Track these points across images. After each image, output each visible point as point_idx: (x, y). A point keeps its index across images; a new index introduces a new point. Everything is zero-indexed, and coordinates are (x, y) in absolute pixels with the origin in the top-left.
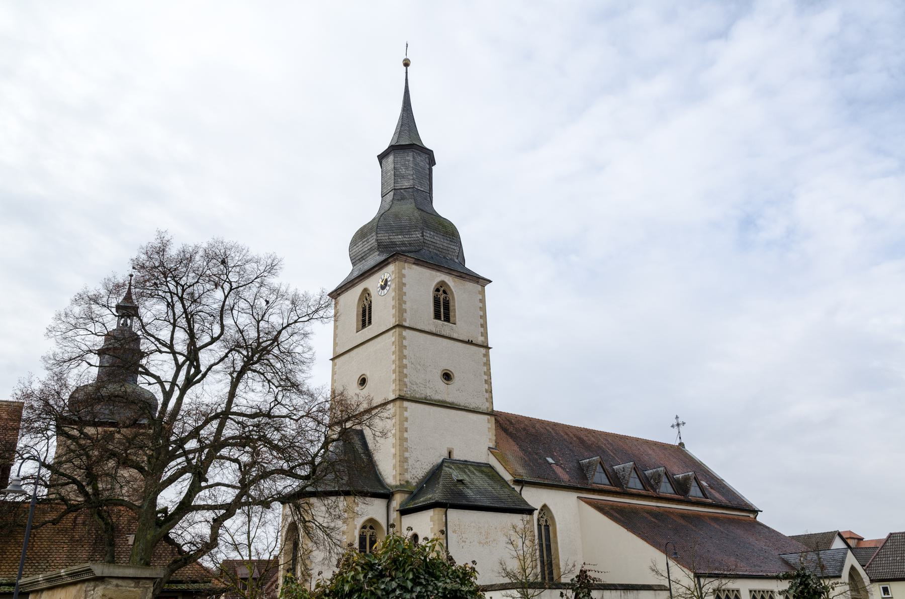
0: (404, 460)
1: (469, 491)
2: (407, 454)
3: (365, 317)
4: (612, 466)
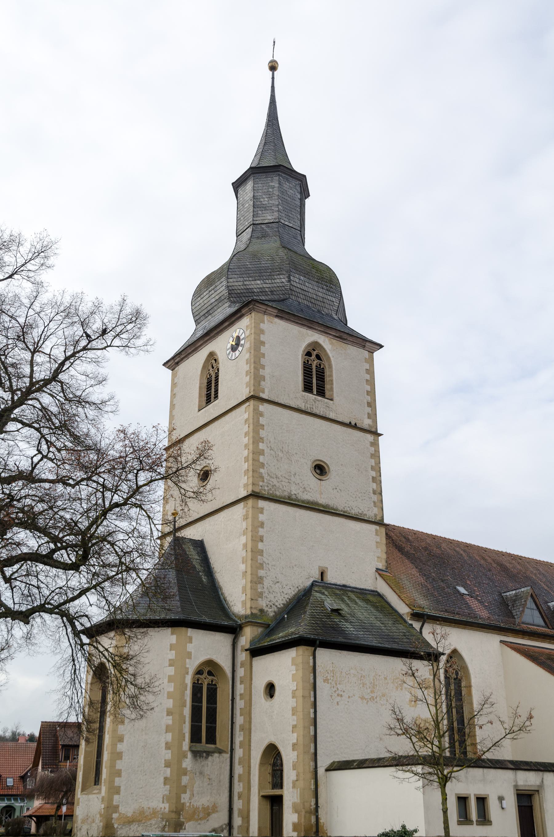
0: (257, 580)
1: (348, 625)
2: (261, 573)
3: (210, 390)
4: (547, 602)
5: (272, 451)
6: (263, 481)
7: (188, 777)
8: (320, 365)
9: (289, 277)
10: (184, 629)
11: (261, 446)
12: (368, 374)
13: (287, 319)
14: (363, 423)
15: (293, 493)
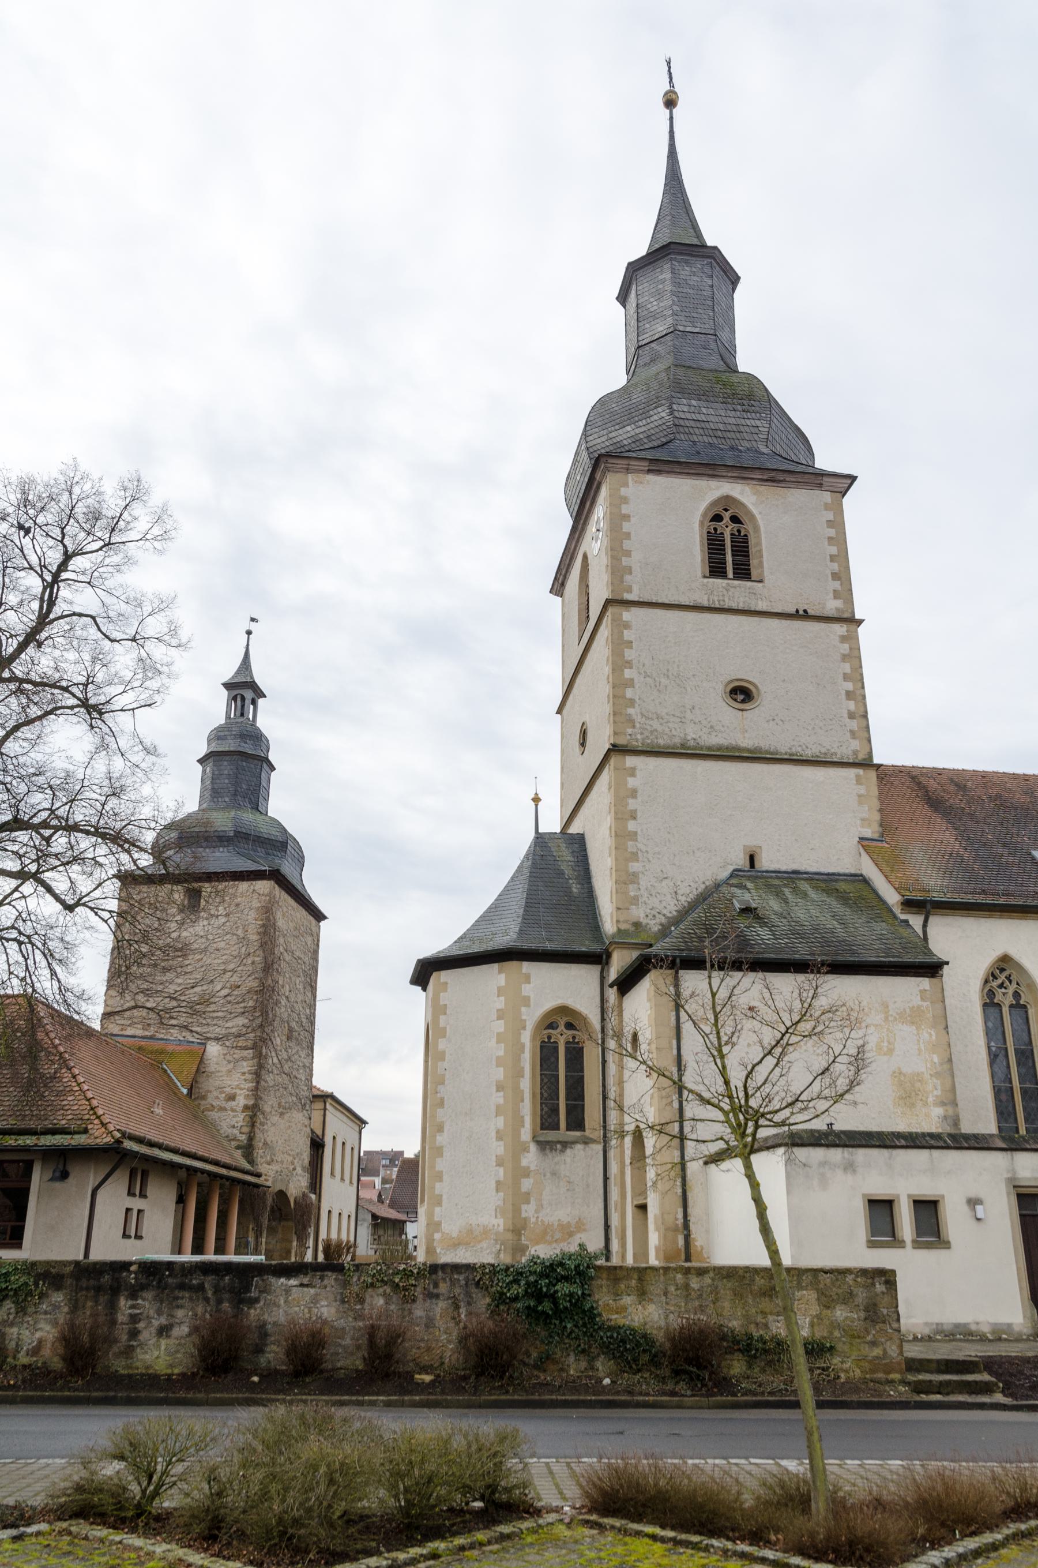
2: (634, 867)
5: (648, 679)
6: (634, 727)
7: (531, 1180)
8: (739, 531)
9: (670, 408)
10: (515, 963)
11: (628, 673)
12: (832, 527)
13: (668, 472)
14: (823, 608)
15: (689, 738)
